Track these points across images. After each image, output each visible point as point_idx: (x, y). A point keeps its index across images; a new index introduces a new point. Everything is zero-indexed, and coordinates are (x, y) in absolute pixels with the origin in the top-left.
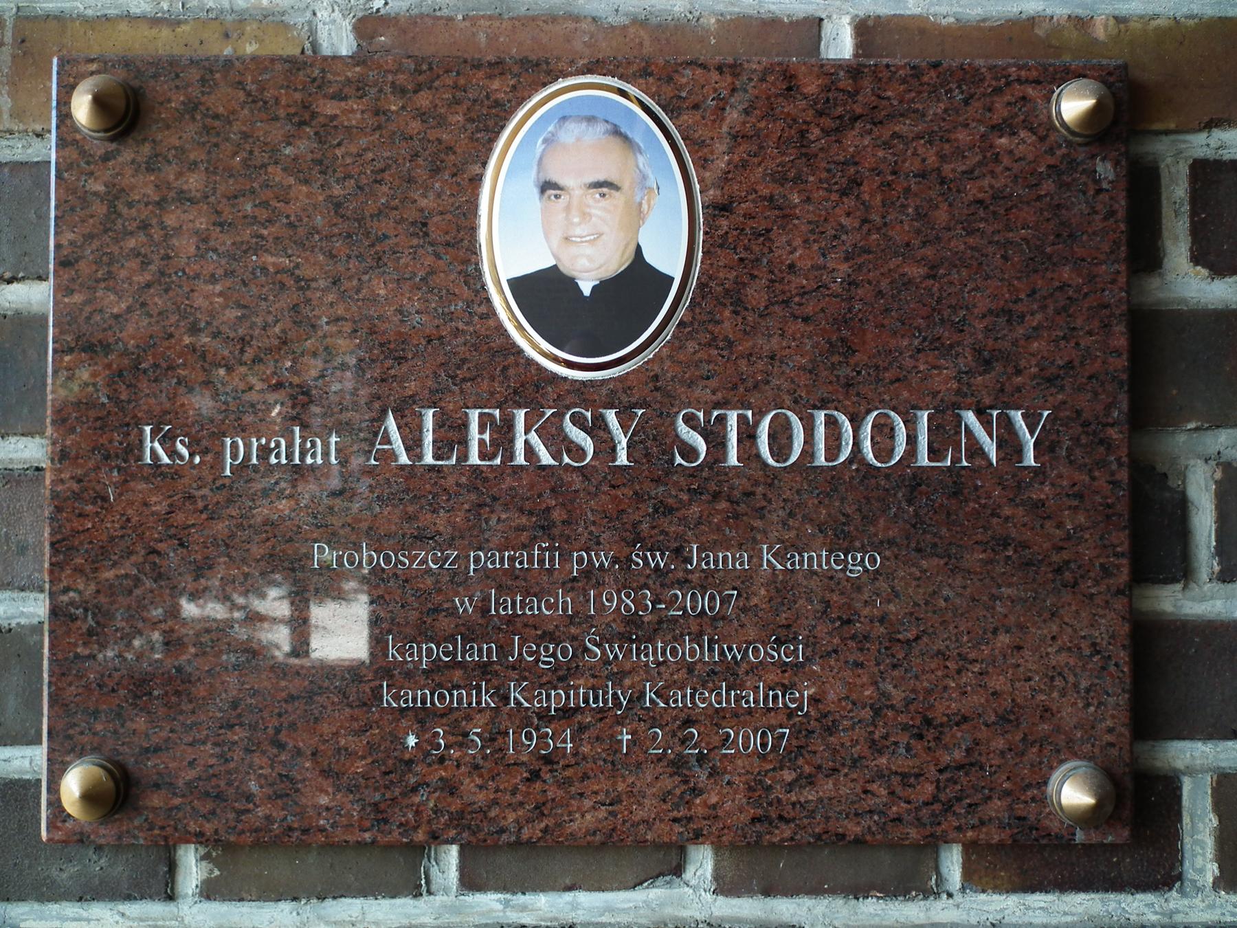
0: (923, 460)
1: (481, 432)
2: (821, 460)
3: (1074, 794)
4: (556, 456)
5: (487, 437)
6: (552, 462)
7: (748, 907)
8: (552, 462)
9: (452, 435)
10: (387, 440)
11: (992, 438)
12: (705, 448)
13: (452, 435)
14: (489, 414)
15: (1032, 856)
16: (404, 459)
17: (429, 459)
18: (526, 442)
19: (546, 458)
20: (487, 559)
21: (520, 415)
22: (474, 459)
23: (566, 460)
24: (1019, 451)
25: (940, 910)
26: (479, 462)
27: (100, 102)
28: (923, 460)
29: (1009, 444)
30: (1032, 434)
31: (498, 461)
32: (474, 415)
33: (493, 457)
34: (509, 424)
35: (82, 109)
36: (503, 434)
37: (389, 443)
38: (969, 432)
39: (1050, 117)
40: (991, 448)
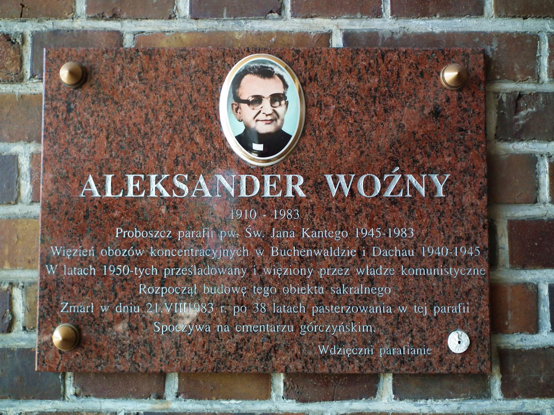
0: (267, 194)
1: (271, 183)
2: (243, 194)
3: (457, 342)
4: (170, 193)
5: (137, 185)
6: (168, 195)
7: (406, 406)
8: (168, 195)
9: (119, 184)
10: (89, 186)
11: (348, 186)
12: (378, 191)
13: (119, 184)
14: (139, 177)
15: (424, 378)
16: (97, 194)
17: (109, 194)
18: (156, 188)
19: (166, 194)
20: (185, 234)
21: (153, 177)
22: (130, 194)
23: (175, 195)
24: (435, 191)
25: (484, 405)
26: (246, 196)
27: (72, 73)
28: (267, 194)
29: (431, 189)
30: (422, 185)
31: (121, 195)
32: (131, 177)
33: (140, 193)
34: (147, 179)
35: (64, 74)
36: (146, 186)
37: (90, 188)
38: (411, 185)
39: (442, 85)
40: (423, 191)
